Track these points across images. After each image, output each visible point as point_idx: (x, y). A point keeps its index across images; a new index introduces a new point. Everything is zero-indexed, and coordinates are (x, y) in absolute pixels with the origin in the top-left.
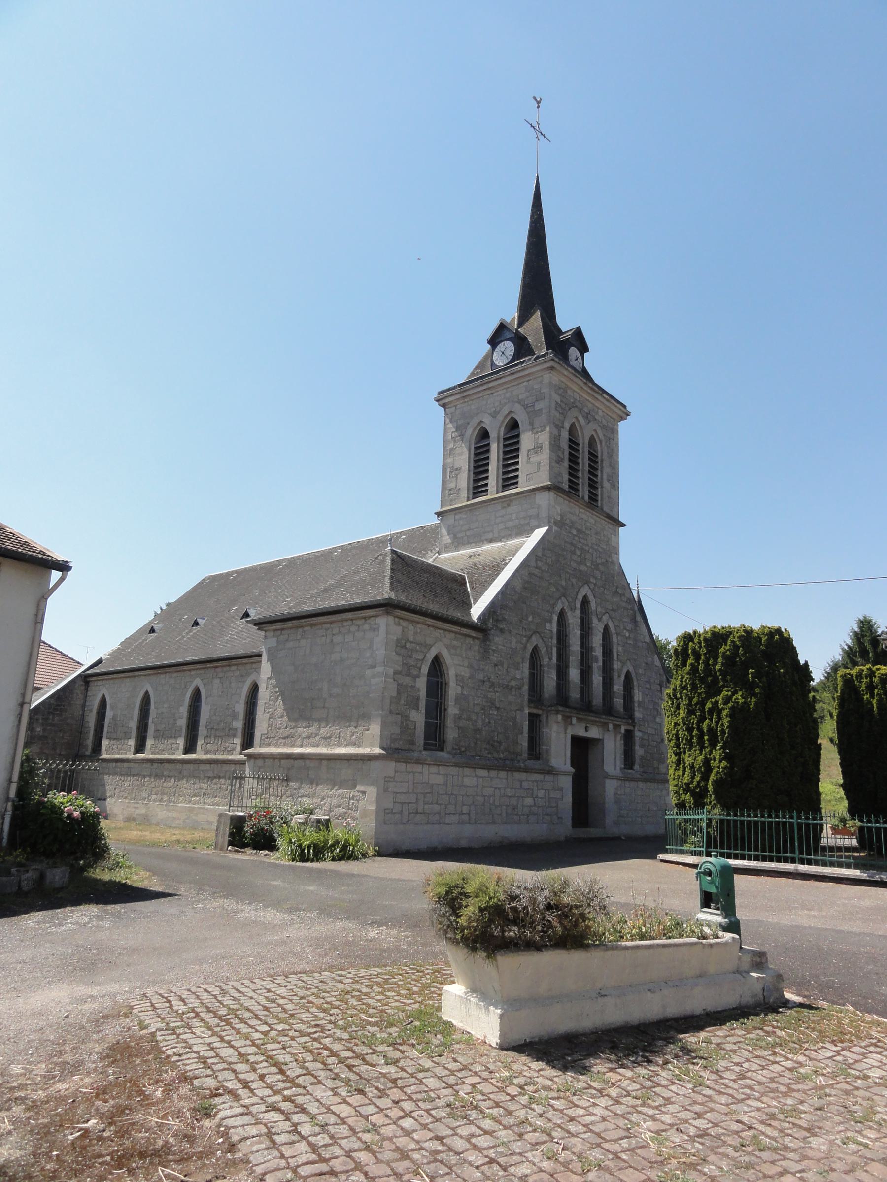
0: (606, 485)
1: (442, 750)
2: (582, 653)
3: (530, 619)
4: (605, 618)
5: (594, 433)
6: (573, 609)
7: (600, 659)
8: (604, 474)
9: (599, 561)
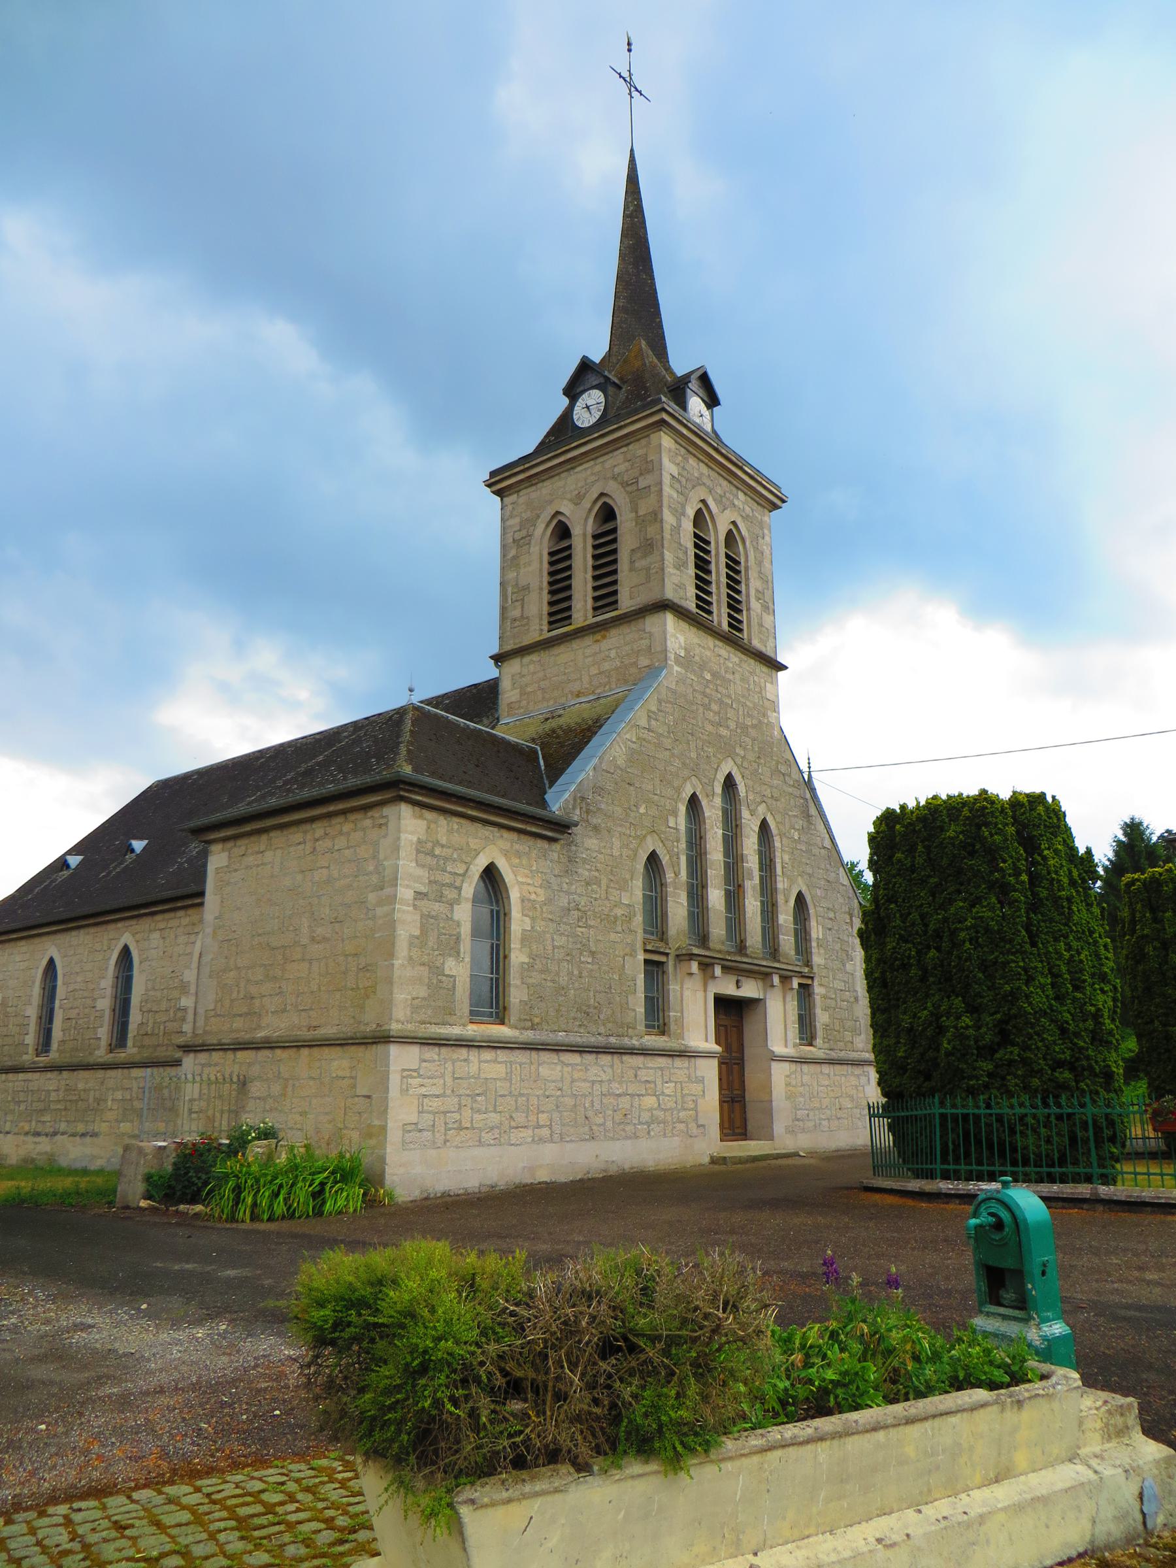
0: (755, 605)
1: (503, 1023)
2: (727, 865)
3: (642, 810)
4: (762, 809)
5: (732, 527)
6: (710, 795)
7: (756, 874)
8: (752, 585)
9: (748, 722)
